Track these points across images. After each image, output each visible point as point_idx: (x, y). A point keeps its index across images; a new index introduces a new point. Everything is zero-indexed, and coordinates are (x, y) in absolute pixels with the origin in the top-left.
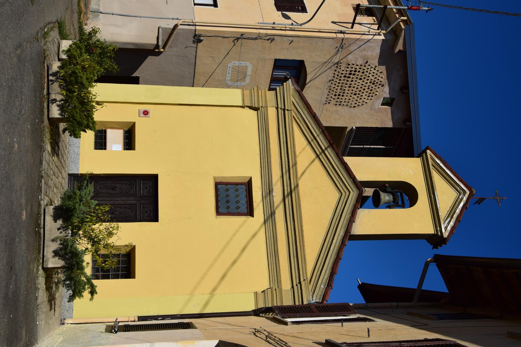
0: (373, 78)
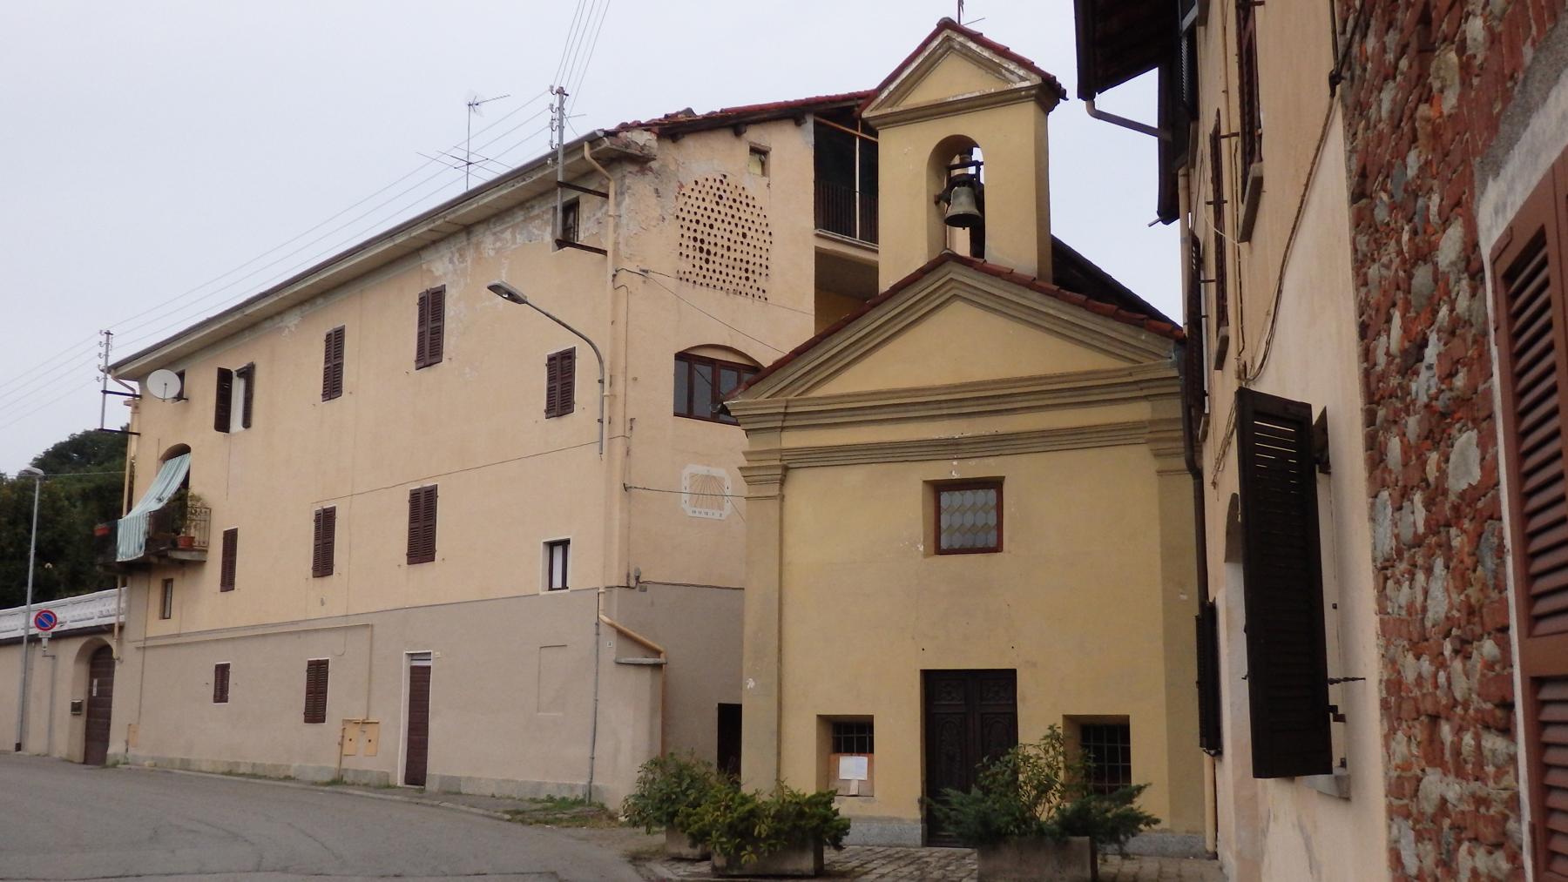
0: (707, 200)
